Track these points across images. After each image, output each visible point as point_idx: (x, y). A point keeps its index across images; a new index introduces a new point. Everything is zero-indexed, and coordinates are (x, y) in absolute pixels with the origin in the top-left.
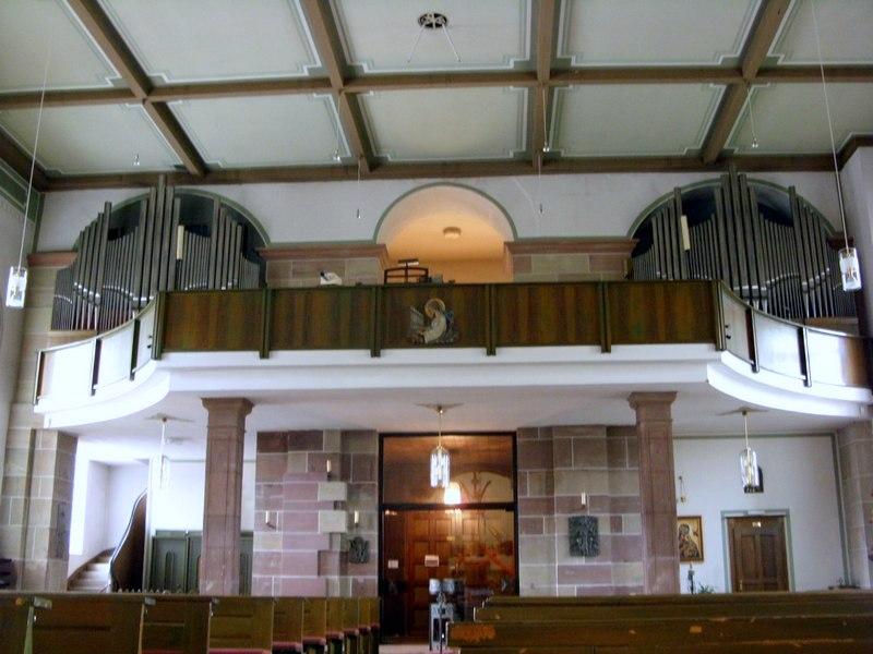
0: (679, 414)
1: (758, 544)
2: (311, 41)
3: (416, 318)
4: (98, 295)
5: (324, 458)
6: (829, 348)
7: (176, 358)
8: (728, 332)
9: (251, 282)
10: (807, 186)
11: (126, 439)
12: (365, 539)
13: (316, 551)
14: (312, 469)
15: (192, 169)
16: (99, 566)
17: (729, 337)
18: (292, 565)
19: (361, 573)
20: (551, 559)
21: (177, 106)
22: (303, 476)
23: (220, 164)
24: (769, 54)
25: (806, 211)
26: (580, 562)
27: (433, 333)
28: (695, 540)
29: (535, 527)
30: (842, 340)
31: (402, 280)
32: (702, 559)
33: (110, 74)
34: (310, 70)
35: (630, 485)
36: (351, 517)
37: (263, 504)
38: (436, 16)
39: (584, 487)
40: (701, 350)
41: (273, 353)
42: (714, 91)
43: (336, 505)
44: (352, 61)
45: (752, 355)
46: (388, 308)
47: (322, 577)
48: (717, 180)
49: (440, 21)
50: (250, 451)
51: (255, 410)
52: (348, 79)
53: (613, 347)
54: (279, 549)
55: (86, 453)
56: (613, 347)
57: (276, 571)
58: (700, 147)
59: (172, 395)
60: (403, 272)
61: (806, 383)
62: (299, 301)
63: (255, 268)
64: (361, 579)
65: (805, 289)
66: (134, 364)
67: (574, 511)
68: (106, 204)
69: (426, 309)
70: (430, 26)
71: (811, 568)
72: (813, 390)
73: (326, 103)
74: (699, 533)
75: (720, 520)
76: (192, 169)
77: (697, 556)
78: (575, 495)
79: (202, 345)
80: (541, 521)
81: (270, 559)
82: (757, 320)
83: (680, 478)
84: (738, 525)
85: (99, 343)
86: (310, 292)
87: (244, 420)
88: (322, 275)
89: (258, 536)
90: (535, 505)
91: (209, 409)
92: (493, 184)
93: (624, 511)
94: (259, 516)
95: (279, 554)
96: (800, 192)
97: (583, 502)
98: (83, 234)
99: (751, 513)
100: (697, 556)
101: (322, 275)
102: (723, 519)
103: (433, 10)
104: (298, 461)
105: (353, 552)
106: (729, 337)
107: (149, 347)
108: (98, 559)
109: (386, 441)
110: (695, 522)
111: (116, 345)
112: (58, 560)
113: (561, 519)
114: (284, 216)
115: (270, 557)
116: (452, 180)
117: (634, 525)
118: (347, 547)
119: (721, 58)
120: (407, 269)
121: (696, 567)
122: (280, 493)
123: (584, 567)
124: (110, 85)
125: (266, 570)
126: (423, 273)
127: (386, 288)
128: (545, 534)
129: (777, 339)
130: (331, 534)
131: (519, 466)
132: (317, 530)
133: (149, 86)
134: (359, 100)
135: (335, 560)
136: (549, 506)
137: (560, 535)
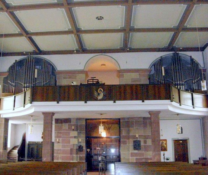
0: (160, 115)
1: (181, 147)
2: (67, 19)
3: (96, 94)
4: (14, 84)
5: (72, 125)
6: (199, 98)
7: (35, 103)
8: (174, 97)
9: (53, 83)
10: (197, 56)
11: (21, 117)
12: (82, 146)
13: (70, 149)
14: (69, 128)
15: (37, 51)
16: (14, 150)
17: (174, 98)
18: (64, 152)
19: (81, 154)
20: (129, 150)
21: (34, 38)
22: (66, 130)
23: (44, 50)
24: (185, 25)
25: (194, 62)
26: (136, 151)
27: (100, 97)
28: (165, 145)
29: (125, 143)
30: (203, 96)
31: (92, 83)
32: (167, 150)
33: (17, 30)
34: (68, 29)
35: (148, 132)
36: (79, 140)
37: (57, 137)
38: (101, 17)
39: (137, 133)
40: (168, 101)
41: (60, 102)
42: (172, 33)
43: (75, 137)
44: (79, 27)
45: (180, 102)
46: (87, 91)
47: (72, 155)
48: (172, 54)
49: (102, 18)
50: (54, 122)
51: (55, 115)
52: (77, 31)
53: (145, 101)
54: (60, 148)
55: (10, 122)
56: (145, 101)
57: (60, 153)
58: (167, 45)
59: (34, 112)
60: (92, 81)
61: (194, 108)
62: (67, 88)
63: (54, 77)
64: (81, 155)
65: (194, 82)
66: (24, 104)
67: (134, 139)
68: (16, 60)
69: (98, 91)
70: (99, 19)
71: (195, 153)
72: (196, 109)
73: (72, 37)
74: (166, 144)
75: (171, 140)
76: (37, 51)
77: (165, 149)
78: (135, 135)
79: (42, 100)
80: (126, 141)
81: (59, 150)
82: (181, 92)
83: (162, 130)
84: (177, 143)
85: (15, 97)
86: (69, 87)
87: (52, 117)
88: (72, 83)
89: (55, 145)
90: (125, 137)
91: (44, 115)
92: (115, 55)
93: (147, 139)
94: (56, 140)
95: (61, 149)
96: (193, 57)
97: (137, 136)
98: (10, 68)
99: (179, 139)
100: (165, 149)
101: (72, 83)
102: (172, 140)
103: (99, 16)
104: (65, 126)
105: (80, 148)
106: (174, 98)
107: (29, 100)
108: (14, 148)
109: (87, 120)
110: (165, 141)
111: (20, 97)
112: (5, 150)
113: (131, 140)
114: (61, 63)
115: (58, 150)
116: (104, 54)
117: (149, 142)
118: (78, 148)
119: (173, 26)
120: (93, 80)
121: (165, 152)
122: (61, 134)
123: (137, 153)
124: (17, 33)
125: (58, 153)
126: (97, 81)
127: (89, 85)
128: (127, 144)
129: (186, 96)
130: (74, 144)
131: (121, 127)
132: (70, 143)
133: (27, 33)
134: (81, 36)
135: (75, 151)
136: (128, 137)
137: (131, 145)
